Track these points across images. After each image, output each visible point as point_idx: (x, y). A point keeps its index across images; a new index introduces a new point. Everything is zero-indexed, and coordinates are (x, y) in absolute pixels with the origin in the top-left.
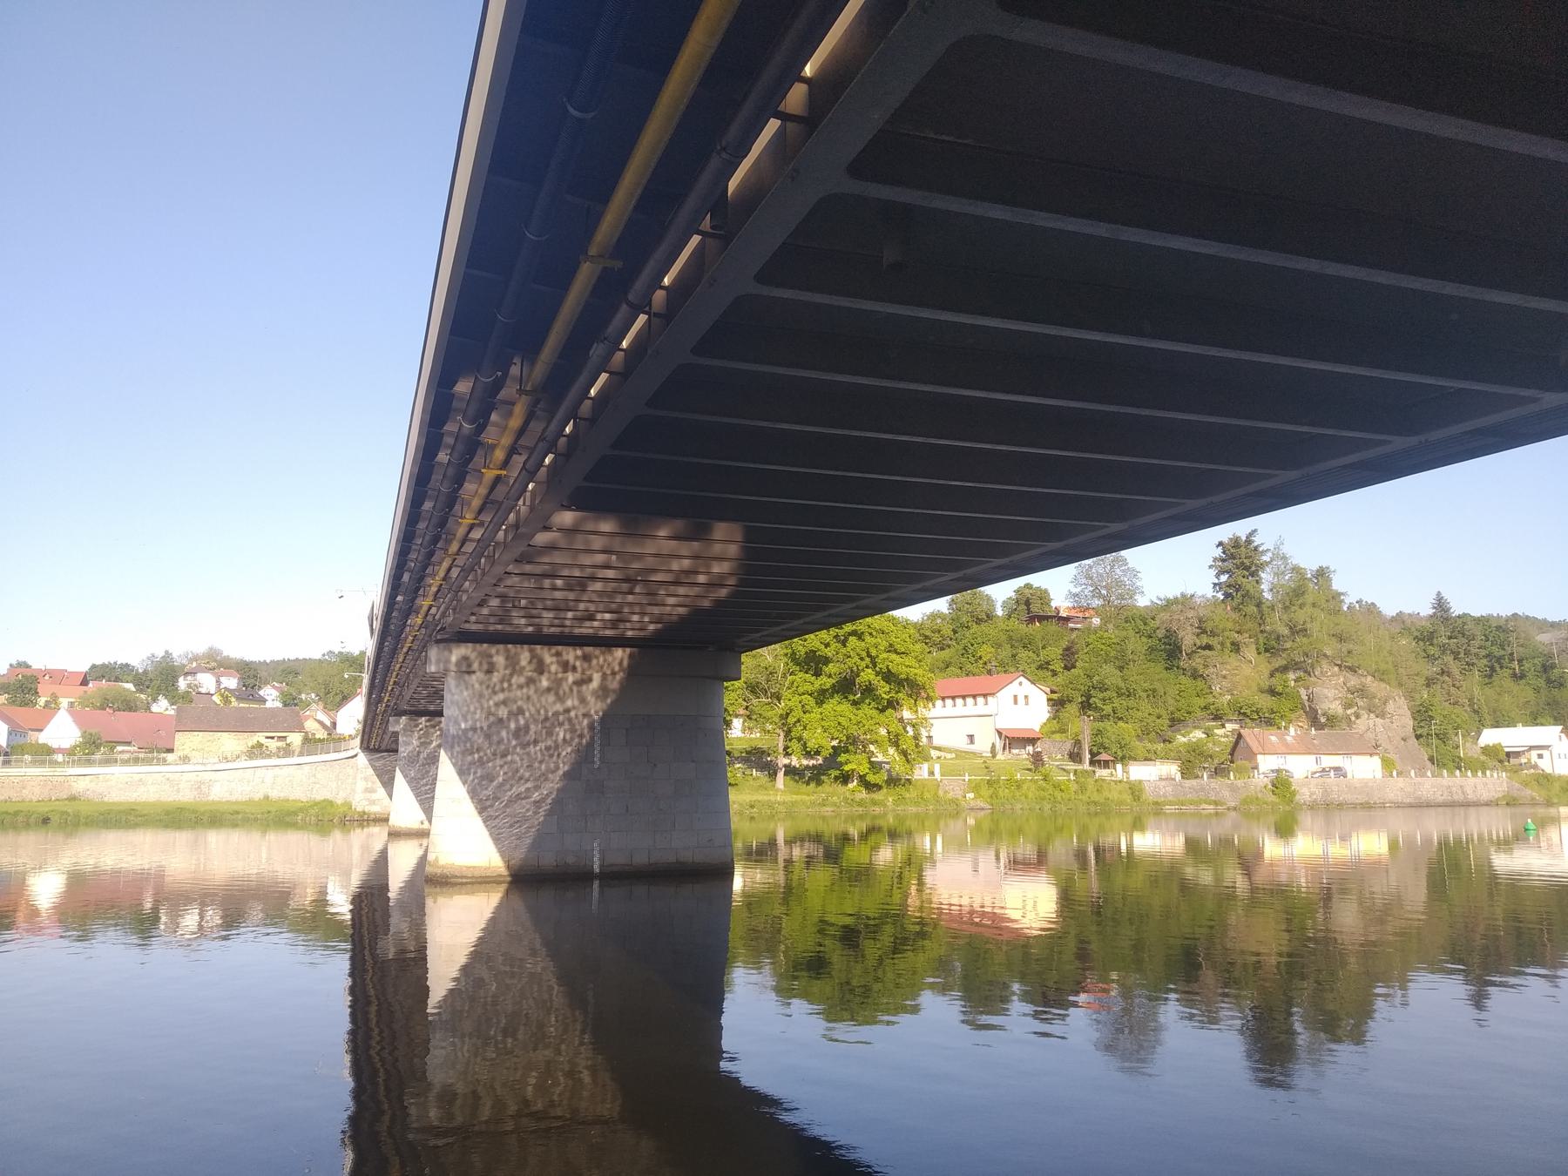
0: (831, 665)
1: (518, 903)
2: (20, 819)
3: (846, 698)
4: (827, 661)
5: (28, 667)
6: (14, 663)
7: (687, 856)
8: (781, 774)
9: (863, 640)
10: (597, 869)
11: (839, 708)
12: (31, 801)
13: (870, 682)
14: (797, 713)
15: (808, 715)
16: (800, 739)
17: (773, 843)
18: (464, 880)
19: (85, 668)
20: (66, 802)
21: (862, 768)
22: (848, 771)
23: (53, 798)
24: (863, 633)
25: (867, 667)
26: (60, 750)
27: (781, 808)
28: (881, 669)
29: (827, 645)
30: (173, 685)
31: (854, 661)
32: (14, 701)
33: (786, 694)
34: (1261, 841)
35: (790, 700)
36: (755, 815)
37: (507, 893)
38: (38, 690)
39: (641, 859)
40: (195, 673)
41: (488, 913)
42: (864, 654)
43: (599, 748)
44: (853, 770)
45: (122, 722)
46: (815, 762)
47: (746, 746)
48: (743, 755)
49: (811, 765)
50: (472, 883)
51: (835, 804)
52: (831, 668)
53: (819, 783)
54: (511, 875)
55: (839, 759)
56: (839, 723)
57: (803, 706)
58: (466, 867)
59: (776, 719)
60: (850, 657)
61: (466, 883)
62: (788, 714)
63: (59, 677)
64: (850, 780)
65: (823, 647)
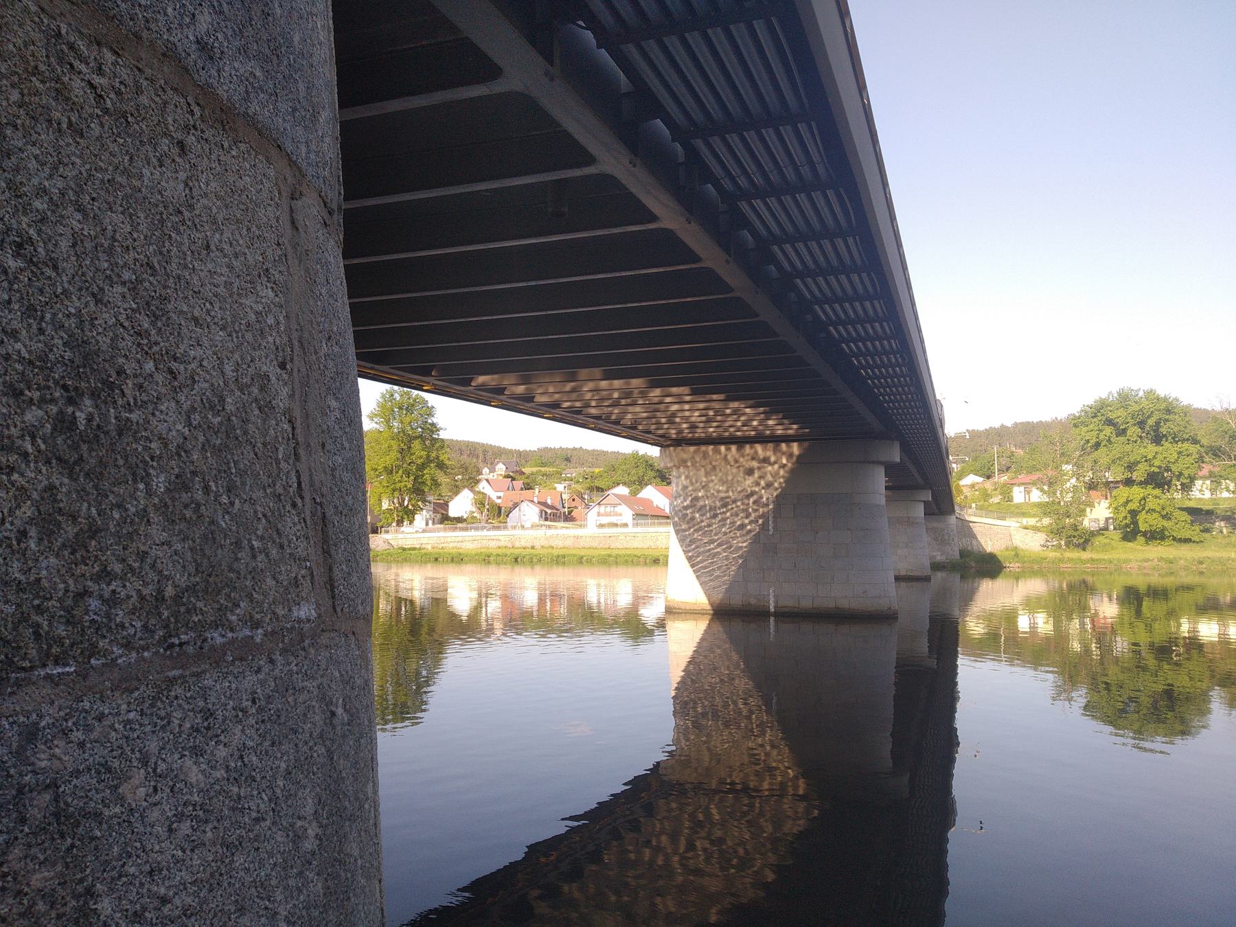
1: (718, 628)
7: (844, 604)
10: (772, 609)
37: (711, 621)
39: (806, 604)
50: (685, 613)
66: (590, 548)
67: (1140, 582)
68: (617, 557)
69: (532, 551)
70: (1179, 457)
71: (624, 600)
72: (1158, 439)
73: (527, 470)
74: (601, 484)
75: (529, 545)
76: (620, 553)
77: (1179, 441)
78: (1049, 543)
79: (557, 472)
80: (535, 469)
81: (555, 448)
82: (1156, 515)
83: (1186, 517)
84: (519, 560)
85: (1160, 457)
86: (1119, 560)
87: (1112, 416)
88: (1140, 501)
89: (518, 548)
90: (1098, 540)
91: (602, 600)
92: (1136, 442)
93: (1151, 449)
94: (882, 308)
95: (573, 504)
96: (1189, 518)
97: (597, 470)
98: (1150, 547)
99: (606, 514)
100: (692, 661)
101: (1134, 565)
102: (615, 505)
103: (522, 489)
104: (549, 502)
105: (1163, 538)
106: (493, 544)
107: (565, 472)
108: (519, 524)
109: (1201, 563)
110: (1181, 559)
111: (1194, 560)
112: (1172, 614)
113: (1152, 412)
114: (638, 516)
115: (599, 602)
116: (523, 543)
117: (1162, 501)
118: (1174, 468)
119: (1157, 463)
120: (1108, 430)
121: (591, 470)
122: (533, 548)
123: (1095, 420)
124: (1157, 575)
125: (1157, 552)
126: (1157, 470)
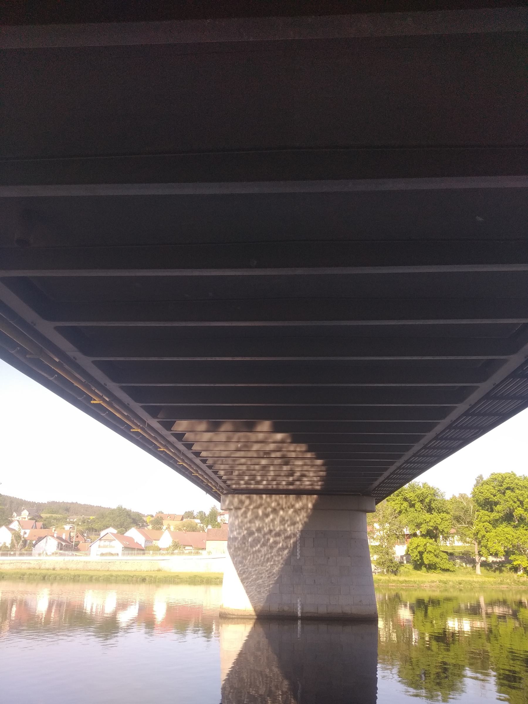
0: (498, 506)
1: (260, 630)
2: (134, 579)
3: (509, 524)
4: (496, 504)
5: (162, 513)
6: (158, 512)
7: (348, 610)
8: (478, 566)
9: (514, 492)
10: (299, 614)
11: (505, 530)
12: (144, 571)
13: (521, 515)
14: (483, 532)
15: (488, 533)
16: (486, 547)
17: (479, 606)
18: (234, 616)
19: (182, 513)
20: (156, 572)
21: (524, 563)
22: (516, 565)
23: (152, 570)
24: (513, 488)
25: (519, 507)
26: (163, 549)
27: (477, 585)
28: (526, 507)
29: (495, 496)
30: (215, 520)
31: (510, 503)
32: (154, 528)
33: (475, 522)
34: (100, 624)
35: (478, 525)
36: (462, 588)
37: (255, 624)
38: (163, 523)
39: (322, 610)
40: (224, 515)
41: (246, 634)
42: (516, 500)
43: (299, 552)
44: (519, 565)
45: (190, 536)
46: (500, 560)
47: (463, 550)
48: (461, 555)
49: (498, 561)
50: (237, 618)
51: (508, 584)
52: (499, 508)
53: (501, 571)
54: (257, 615)
55: (510, 558)
56: (507, 538)
57: (486, 528)
58: (235, 610)
59: (472, 536)
60: (508, 501)
61: (234, 618)
62: (477, 533)
63: (173, 517)
64: (518, 570)
65: (492, 496)
66: (95, 570)
67: (425, 595)
68: (117, 576)
69: (54, 572)
70: (441, 522)
71: (109, 609)
72: (430, 510)
73: (43, 515)
74: (96, 526)
75: (51, 567)
76: (119, 573)
77: (441, 512)
78: (376, 571)
79: (64, 518)
80: (48, 515)
81: (59, 502)
82: (432, 555)
83: (445, 556)
84: (46, 578)
85: (433, 521)
86: (419, 581)
87: (408, 496)
88: (424, 546)
89: (43, 569)
90: (402, 569)
91: (94, 610)
92: (420, 511)
93: (428, 516)
94: (508, 411)
95: (78, 539)
96: (447, 557)
97: (91, 517)
98: (429, 574)
99: (105, 547)
100: (240, 654)
101: (427, 584)
102: (111, 541)
103: (41, 528)
104: (64, 537)
105: (435, 569)
106: (24, 566)
107: (69, 518)
108: (45, 552)
109: (460, 584)
110: (450, 581)
111: (457, 582)
112: (443, 617)
113: (428, 495)
114: (126, 548)
115: (91, 612)
116: (47, 566)
117: (434, 546)
118: (440, 528)
119: (431, 524)
120: (406, 504)
121: (88, 517)
122: (54, 569)
123: (399, 498)
124: (439, 591)
125: (435, 577)
126: (431, 528)
